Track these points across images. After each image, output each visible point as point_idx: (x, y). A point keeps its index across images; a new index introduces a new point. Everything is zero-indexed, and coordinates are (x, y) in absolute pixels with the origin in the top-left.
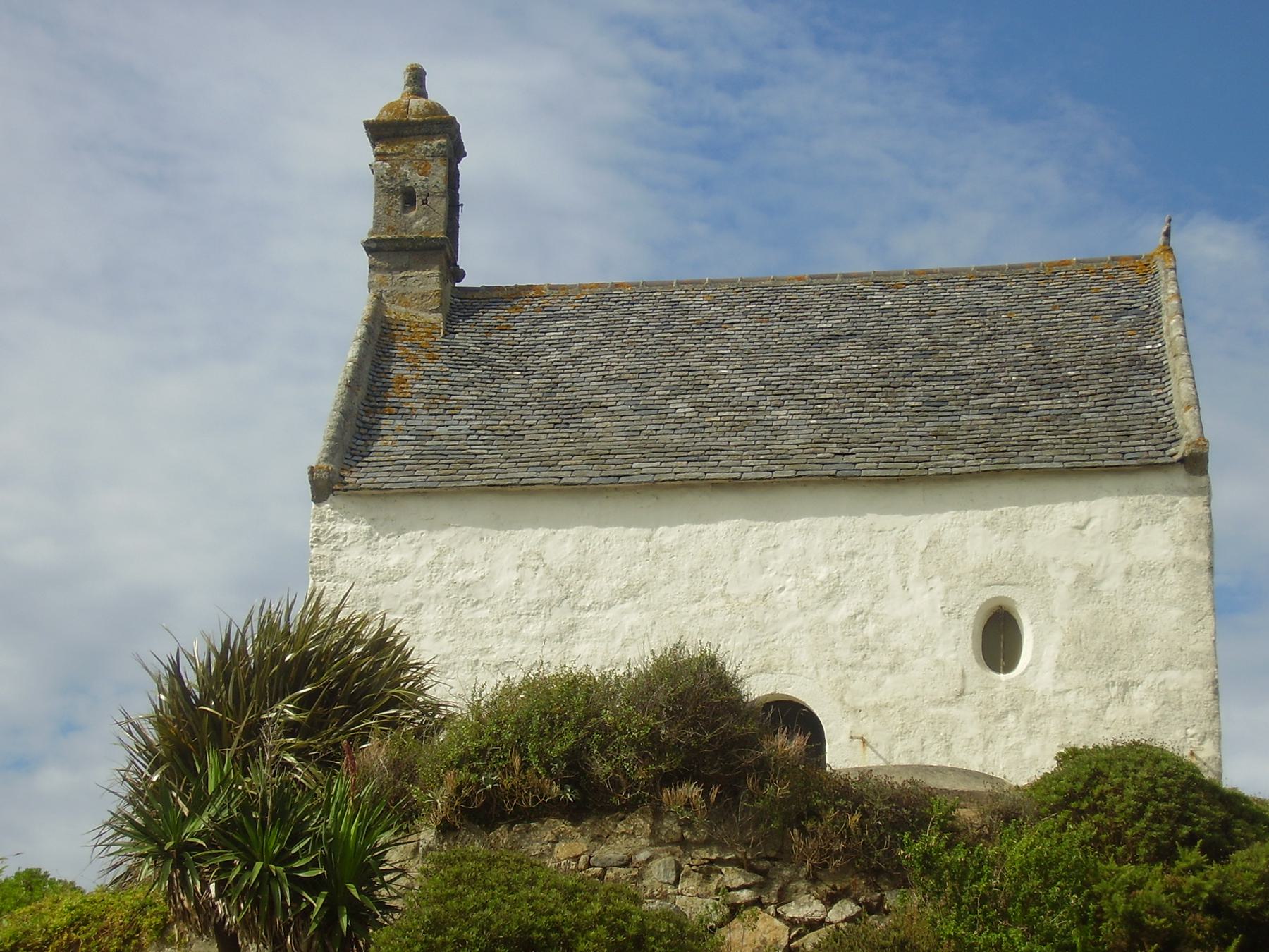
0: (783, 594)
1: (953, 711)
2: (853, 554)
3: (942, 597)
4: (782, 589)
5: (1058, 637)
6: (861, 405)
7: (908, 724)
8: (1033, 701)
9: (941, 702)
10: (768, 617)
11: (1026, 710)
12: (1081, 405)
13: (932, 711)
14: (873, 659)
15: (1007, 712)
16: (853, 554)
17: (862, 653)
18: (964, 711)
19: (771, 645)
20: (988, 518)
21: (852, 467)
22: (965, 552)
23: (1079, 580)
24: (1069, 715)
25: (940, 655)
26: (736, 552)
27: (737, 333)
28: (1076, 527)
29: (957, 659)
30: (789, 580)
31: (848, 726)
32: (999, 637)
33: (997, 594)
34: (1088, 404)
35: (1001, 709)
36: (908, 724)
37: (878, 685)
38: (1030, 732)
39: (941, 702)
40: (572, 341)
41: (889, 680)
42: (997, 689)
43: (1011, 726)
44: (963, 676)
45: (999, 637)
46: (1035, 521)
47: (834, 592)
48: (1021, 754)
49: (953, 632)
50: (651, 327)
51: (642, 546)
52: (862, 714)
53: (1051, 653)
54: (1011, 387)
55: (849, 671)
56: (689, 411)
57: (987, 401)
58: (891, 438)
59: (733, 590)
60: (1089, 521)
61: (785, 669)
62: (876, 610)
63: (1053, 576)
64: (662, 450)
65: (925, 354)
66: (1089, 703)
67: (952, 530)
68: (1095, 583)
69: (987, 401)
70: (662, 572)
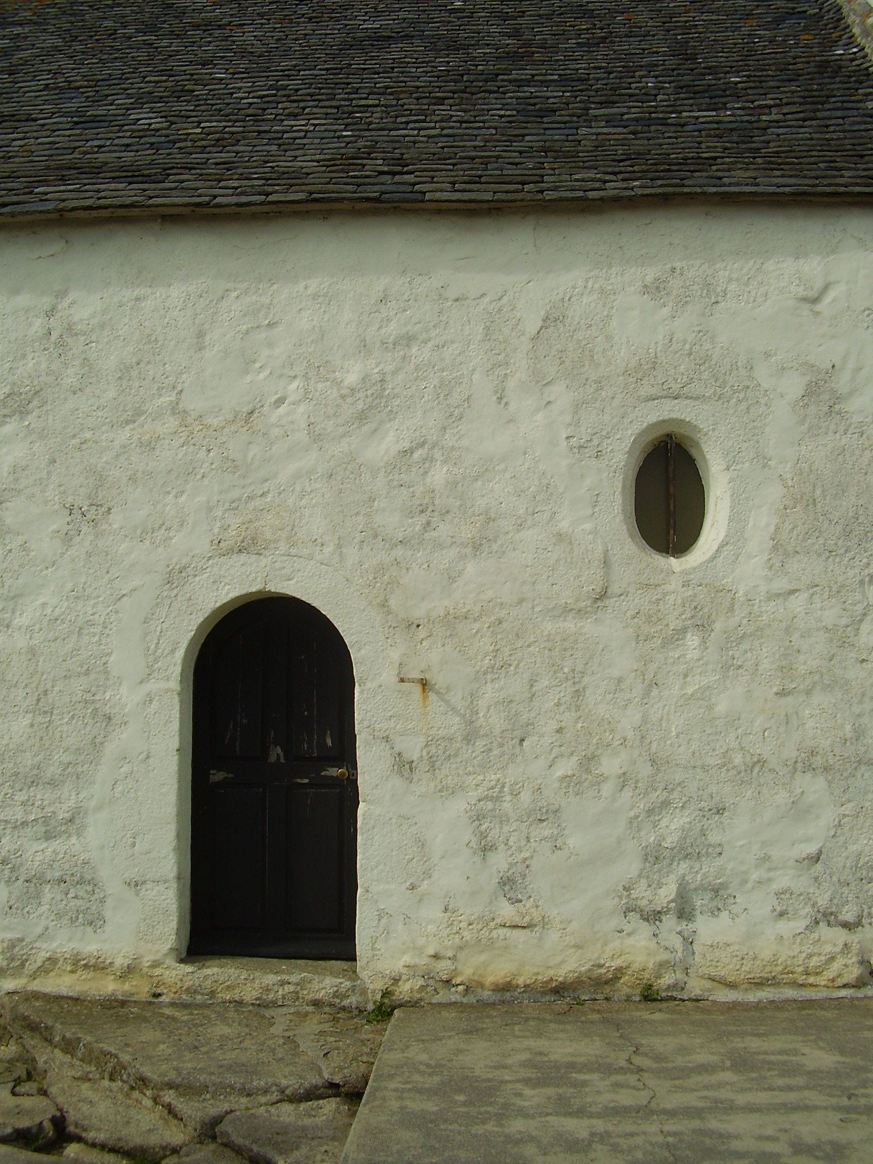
0: (283, 409)
1: (589, 627)
2: (408, 339)
3: (568, 418)
4: (280, 401)
5: (774, 493)
6: (421, 112)
7: (506, 651)
8: (731, 609)
9: (567, 610)
10: (254, 451)
11: (718, 626)
12: (764, 118)
13: (549, 626)
14: (444, 530)
15: (685, 630)
16: (408, 339)
17: (423, 519)
18: (608, 629)
19: (257, 503)
20: (649, 279)
21: (410, 189)
22: (609, 338)
23: (811, 392)
24: (795, 637)
25: (564, 525)
26: (201, 335)
27: (248, 37)
28: (805, 300)
29: (594, 532)
30: (295, 384)
31: (395, 655)
32: (666, 492)
33: (665, 415)
34: (774, 117)
35: (675, 624)
36: (506, 651)
37: (452, 578)
38: (726, 667)
39: (567, 610)
40: (18, 49)
41: (471, 568)
42: (667, 588)
43: (693, 655)
44: (606, 563)
45: (666, 492)
46: (733, 287)
47: (373, 406)
48: (710, 708)
49: (588, 482)
50: (129, 31)
51: (38, 324)
52: (422, 633)
53: (762, 522)
54: (647, 95)
55: (399, 552)
56: (157, 123)
57: (616, 110)
58: (473, 154)
59: (193, 403)
60: (826, 288)
61: (283, 547)
62: (449, 440)
63: (765, 385)
64: (96, 171)
65: (513, 57)
66: (831, 615)
67: (585, 300)
68: (838, 398)
69: (616, 110)
70: (71, 371)
